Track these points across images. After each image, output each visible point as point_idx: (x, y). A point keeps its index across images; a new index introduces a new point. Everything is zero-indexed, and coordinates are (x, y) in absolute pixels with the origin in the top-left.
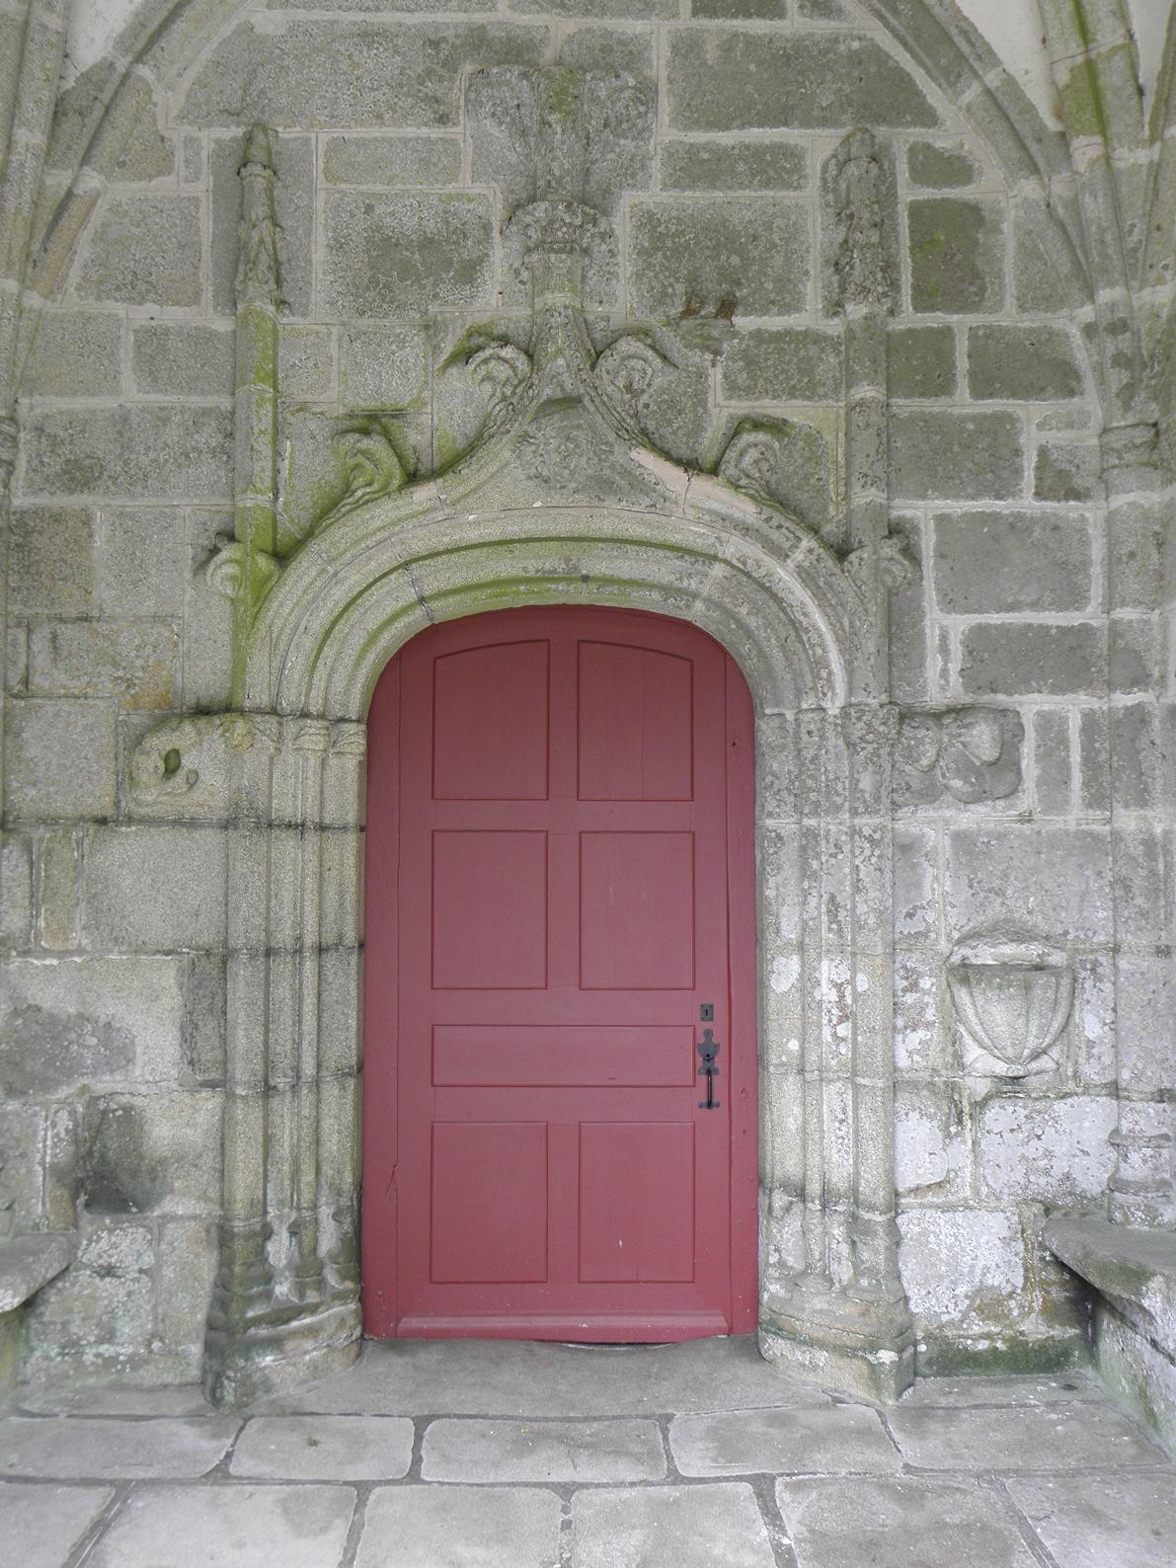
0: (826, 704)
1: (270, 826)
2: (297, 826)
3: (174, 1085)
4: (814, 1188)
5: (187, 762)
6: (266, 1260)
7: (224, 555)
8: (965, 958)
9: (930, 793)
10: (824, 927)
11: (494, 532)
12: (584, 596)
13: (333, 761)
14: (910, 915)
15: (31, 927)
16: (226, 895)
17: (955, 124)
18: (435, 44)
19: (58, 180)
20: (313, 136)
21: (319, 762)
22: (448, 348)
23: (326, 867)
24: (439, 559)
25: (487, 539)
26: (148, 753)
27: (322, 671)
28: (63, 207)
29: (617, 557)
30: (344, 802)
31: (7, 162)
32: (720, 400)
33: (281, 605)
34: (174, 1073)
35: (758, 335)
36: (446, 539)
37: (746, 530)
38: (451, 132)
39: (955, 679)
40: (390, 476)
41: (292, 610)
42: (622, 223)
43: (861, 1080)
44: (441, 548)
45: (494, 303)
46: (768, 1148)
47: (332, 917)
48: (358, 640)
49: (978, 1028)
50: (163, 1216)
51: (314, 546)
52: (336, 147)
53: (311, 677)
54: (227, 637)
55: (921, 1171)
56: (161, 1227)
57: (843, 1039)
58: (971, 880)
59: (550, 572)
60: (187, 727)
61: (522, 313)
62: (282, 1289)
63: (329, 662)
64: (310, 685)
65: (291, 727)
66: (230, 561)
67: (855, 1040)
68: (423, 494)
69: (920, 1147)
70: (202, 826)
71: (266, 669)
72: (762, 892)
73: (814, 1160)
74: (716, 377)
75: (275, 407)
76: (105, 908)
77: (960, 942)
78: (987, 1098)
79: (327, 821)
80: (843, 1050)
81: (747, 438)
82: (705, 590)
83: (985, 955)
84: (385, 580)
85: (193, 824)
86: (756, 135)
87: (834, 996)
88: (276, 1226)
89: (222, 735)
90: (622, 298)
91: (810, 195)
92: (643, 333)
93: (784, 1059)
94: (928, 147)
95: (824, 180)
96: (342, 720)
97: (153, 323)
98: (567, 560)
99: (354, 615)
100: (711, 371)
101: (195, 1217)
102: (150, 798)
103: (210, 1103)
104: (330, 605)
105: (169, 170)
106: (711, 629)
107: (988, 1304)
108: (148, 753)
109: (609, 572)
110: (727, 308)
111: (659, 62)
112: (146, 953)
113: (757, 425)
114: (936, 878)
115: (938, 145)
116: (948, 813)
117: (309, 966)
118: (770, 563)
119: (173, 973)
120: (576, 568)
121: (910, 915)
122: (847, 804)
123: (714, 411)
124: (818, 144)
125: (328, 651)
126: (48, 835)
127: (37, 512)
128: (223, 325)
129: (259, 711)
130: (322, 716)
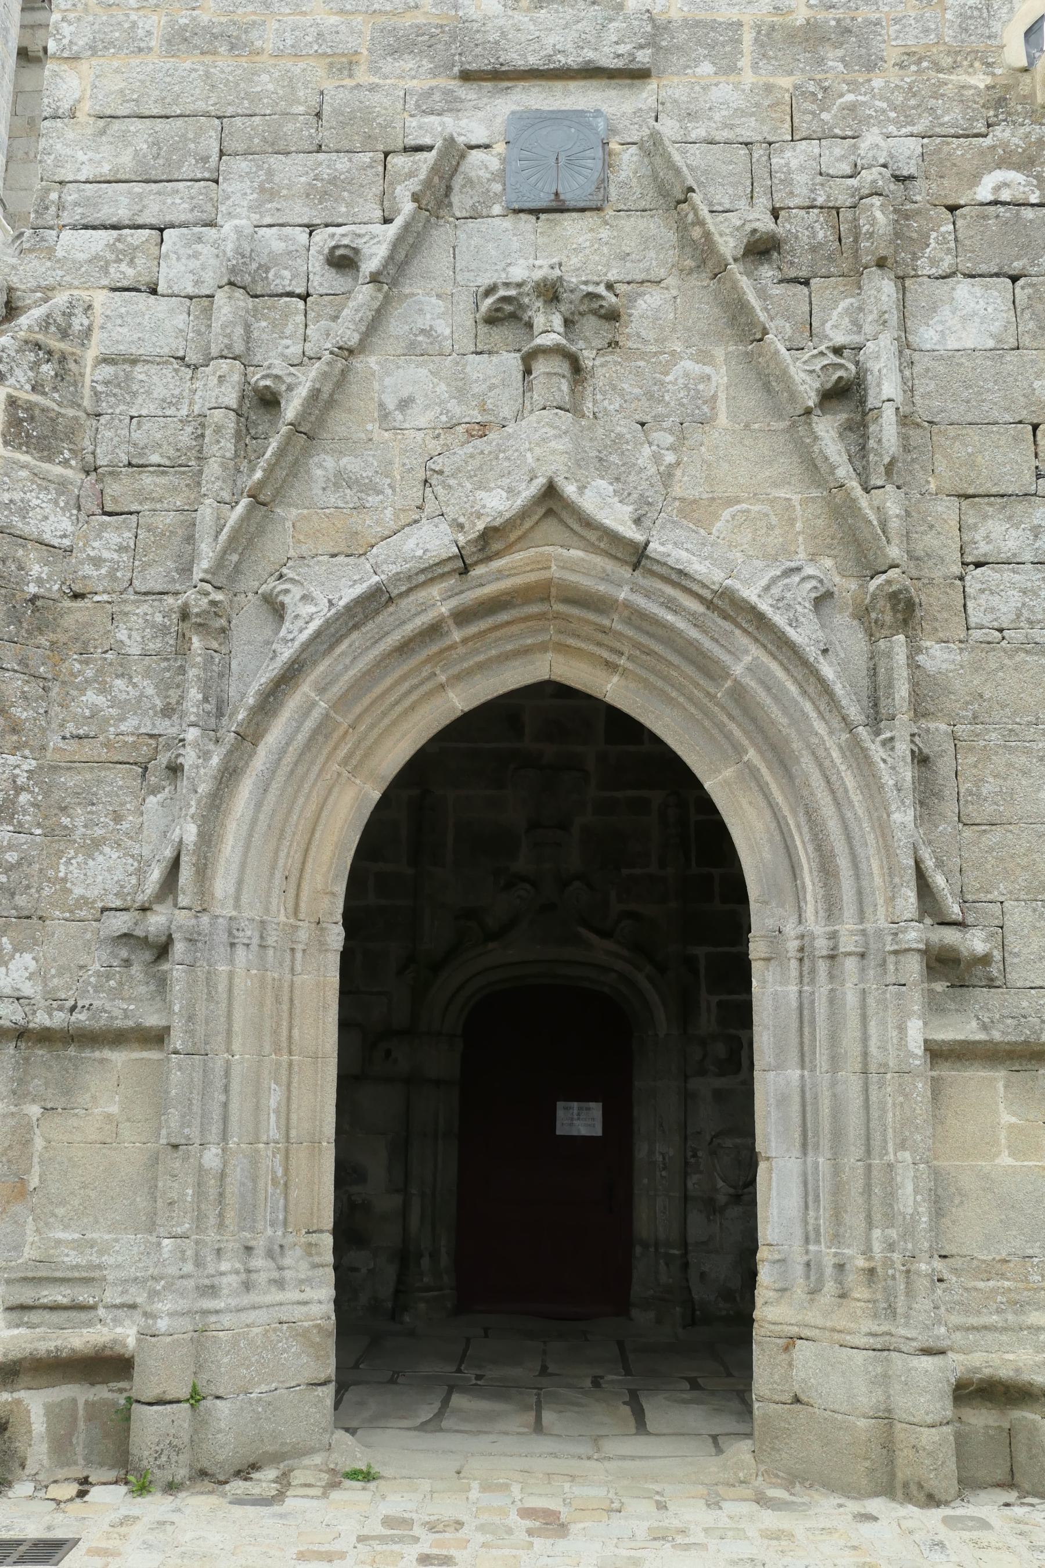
9: (702, 1072)
62: (426, 1280)
86: (630, 793)
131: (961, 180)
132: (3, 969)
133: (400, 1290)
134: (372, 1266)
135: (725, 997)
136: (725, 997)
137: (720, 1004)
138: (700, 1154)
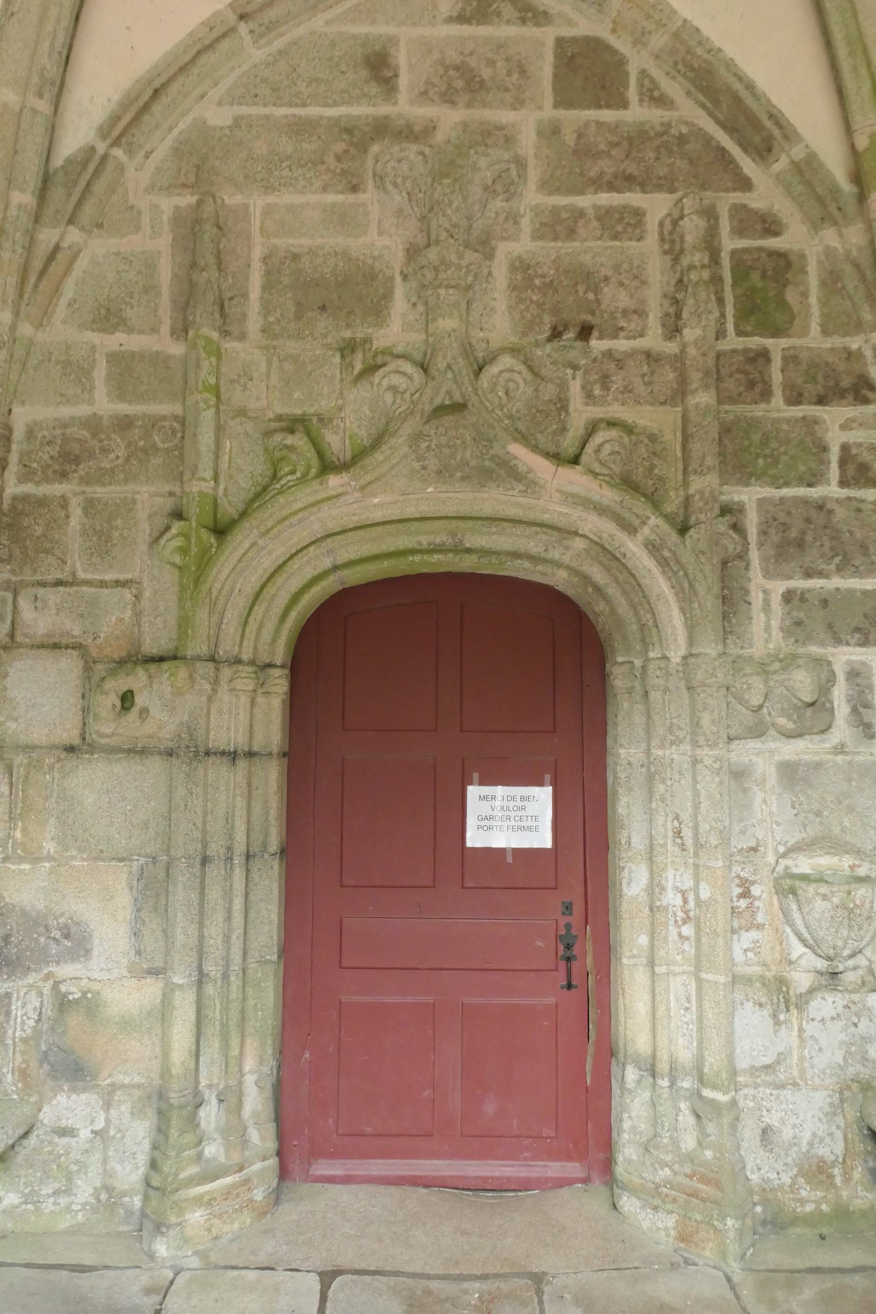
0: (670, 654)
1: (207, 753)
2: (230, 753)
3: (125, 973)
4: (663, 1066)
5: (140, 700)
6: (198, 1125)
7: (174, 531)
8: (787, 868)
9: (758, 731)
10: (669, 842)
11: (395, 513)
12: (466, 564)
13: (260, 699)
14: (743, 832)
15: (9, 837)
16: (170, 812)
17: (766, 192)
18: (349, 131)
19: (47, 236)
20: (251, 202)
21: (249, 700)
22: (358, 367)
23: (254, 786)
24: (350, 534)
25: (389, 519)
26: (107, 694)
27: (252, 626)
28: (52, 257)
29: (494, 533)
30: (272, 731)
31: (5, 218)
32: (580, 407)
33: (219, 571)
34: (124, 961)
35: (609, 354)
36: (355, 518)
37: (601, 510)
38: (361, 197)
39: (777, 634)
40: (309, 468)
41: (228, 576)
43: (703, 975)
44: (351, 526)
46: (621, 1028)
47: (258, 829)
48: (283, 598)
49: (804, 931)
50: (113, 1085)
51: (246, 524)
52: (268, 211)
53: (243, 631)
54: (175, 598)
55: (755, 1053)
56: (111, 1093)
57: (688, 939)
58: (793, 803)
59: (440, 545)
60: (141, 672)
61: (416, 338)
62: (210, 1150)
63: (259, 618)
64: (243, 636)
65: (226, 672)
66: (177, 536)
67: (698, 940)
68: (334, 481)
69: (754, 1034)
70: (152, 753)
71: (206, 624)
72: (614, 810)
73: (663, 1042)
74: (575, 388)
75: (218, 412)
76: (70, 821)
77: (784, 856)
78: (812, 991)
79: (255, 749)
80: (686, 947)
81: (600, 437)
82: (566, 559)
83: (803, 865)
84: (305, 552)
85: (144, 752)
86: (606, 198)
87: (679, 901)
88: (207, 1094)
89: (168, 679)
90: (499, 324)
92: (514, 351)
93: (635, 952)
94: (744, 206)
95: (661, 234)
96: (270, 665)
97: (123, 349)
98: (454, 535)
99: (279, 580)
100: (572, 382)
101: (139, 1086)
102: (108, 731)
103: (152, 989)
104: (260, 572)
105: (138, 229)
106: (570, 592)
107: (817, 1172)
108: (107, 694)
109: (487, 546)
110: (585, 332)
111: (528, 143)
112: (103, 860)
113: (612, 424)
114: (765, 801)
115: (754, 205)
116: (773, 745)
117: (239, 874)
118: (622, 536)
119: (124, 877)
120: (461, 542)
121: (743, 832)
122: (688, 737)
123: (574, 415)
124: (656, 206)
125: (259, 611)
126: (26, 761)
127: (25, 498)
128: (177, 349)
129: (199, 658)
130: (252, 663)
131: (467, 349)
132: (875, 1052)
133: (157, 1184)
134: (100, 1125)
135: (800, 584)
136: (800, 584)
137: (788, 597)
138: (756, 890)
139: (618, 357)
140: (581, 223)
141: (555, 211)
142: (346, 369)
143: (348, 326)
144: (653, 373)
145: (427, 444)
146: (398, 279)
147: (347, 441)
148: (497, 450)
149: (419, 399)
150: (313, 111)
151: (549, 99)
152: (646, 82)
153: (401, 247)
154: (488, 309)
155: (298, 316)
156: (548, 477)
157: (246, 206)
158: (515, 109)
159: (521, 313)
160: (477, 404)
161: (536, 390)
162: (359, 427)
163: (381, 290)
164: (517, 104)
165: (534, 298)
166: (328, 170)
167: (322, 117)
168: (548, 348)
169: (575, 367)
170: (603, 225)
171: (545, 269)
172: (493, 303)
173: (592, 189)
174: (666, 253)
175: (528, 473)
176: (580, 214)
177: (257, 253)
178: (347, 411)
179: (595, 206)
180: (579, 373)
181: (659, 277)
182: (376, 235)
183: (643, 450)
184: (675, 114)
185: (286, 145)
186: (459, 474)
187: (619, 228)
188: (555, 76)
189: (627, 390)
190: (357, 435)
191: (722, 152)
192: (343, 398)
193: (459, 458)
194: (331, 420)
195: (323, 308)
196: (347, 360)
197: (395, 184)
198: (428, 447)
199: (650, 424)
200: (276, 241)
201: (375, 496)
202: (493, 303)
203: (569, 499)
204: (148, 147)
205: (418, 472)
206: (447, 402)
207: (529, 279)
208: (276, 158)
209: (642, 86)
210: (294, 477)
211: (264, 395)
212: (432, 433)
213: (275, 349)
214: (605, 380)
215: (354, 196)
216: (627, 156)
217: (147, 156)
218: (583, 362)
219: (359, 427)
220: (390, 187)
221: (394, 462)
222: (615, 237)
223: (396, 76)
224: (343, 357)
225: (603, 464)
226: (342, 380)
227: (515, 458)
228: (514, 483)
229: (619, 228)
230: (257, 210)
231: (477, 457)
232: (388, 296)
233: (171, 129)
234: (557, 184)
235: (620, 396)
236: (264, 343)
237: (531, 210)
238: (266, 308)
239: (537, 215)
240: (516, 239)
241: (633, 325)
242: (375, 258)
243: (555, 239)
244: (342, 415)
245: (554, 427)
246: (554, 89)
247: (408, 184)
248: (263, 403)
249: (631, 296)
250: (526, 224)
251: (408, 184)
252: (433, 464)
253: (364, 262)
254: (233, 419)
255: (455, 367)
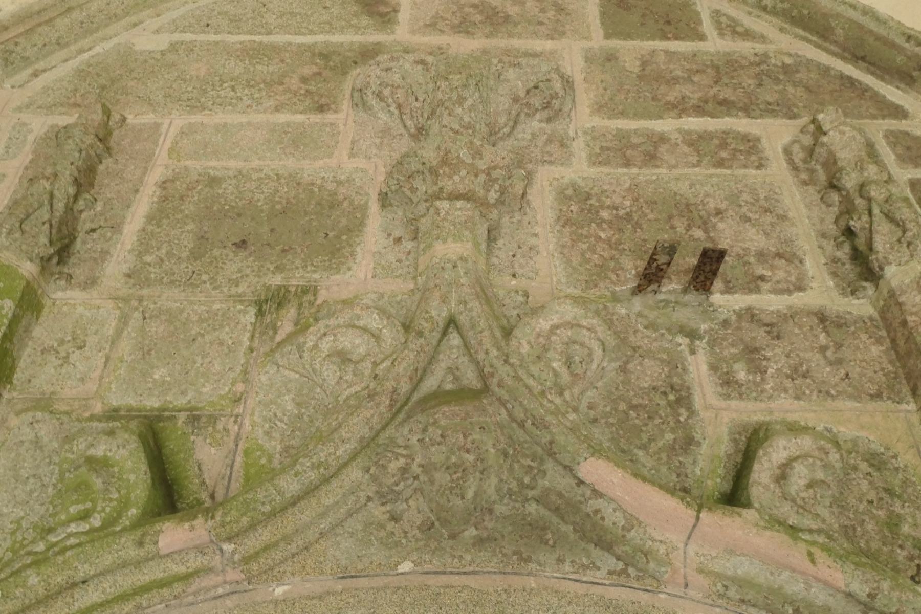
18: (325, 56)
35: (750, 315)
38: (330, 117)
40: (124, 504)
42: (543, 204)
45: (362, 276)
86: (694, 123)
91: (777, 170)
100: (690, 358)
110: (709, 267)
123: (704, 415)
139: (767, 320)
140: (663, 149)
141: (622, 135)
142: (262, 333)
143: (279, 269)
144: (839, 346)
145: (402, 461)
146: (374, 206)
147: (239, 460)
148: (554, 478)
149: (388, 370)
150: (279, 39)
151: (597, 31)
152: (723, 19)
153: (382, 170)
154: (525, 248)
155: (195, 255)
156: (676, 538)
157: (157, 126)
158: (552, 39)
159: (583, 255)
160: (509, 381)
161: (623, 369)
162: (267, 433)
163: (344, 221)
164: (556, 33)
165: (603, 235)
166: (289, 90)
167: (290, 44)
168: (637, 303)
169: (693, 335)
170: (698, 151)
171: (617, 200)
172: (533, 241)
173: (672, 114)
174: (805, 183)
175: (627, 528)
176: (662, 139)
177: (156, 175)
178: (251, 403)
179: (680, 131)
180: (701, 344)
181: (804, 211)
182: (345, 154)
183: (865, 485)
184: (772, 47)
185: (236, 68)
186: (471, 532)
187: (724, 154)
188: (603, 14)
189: (798, 372)
190: (260, 448)
191: (851, 82)
192: (245, 381)
193: (470, 494)
194: (213, 419)
195: (242, 244)
196: (268, 319)
197: (379, 96)
198: (404, 470)
199: (863, 434)
200: (189, 163)
201: (280, 581)
202: (533, 241)
203: (732, 593)
204: (41, 65)
205: (382, 526)
206: (449, 387)
207: (593, 212)
208: (217, 78)
209: (719, 23)
210: (84, 527)
211: (96, 375)
212: (414, 440)
213: (141, 300)
214: (752, 355)
215: (320, 116)
216: (716, 82)
217: (35, 75)
218: (704, 327)
219: (267, 433)
220: (373, 101)
221: (328, 502)
222: (720, 164)
223: (396, 11)
224: (260, 313)
225: (803, 508)
226: (251, 350)
227: (597, 494)
228: (596, 552)
229: (724, 154)
230: (172, 129)
231: (510, 493)
232: (356, 227)
233: (81, 51)
234: (620, 107)
235: (788, 383)
236: (124, 292)
237: (585, 133)
238: (145, 242)
239: (594, 138)
240: (565, 161)
241: (782, 272)
242: (340, 183)
243: (628, 164)
244: (239, 410)
245: (669, 437)
246: (602, 24)
247: (400, 94)
248: (91, 387)
249: (767, 234)
250: (579, 147)
251: (400, 94)
252: (415, 510)
253: (321, 188)
254: (18, 414)
255: (463, 319)
